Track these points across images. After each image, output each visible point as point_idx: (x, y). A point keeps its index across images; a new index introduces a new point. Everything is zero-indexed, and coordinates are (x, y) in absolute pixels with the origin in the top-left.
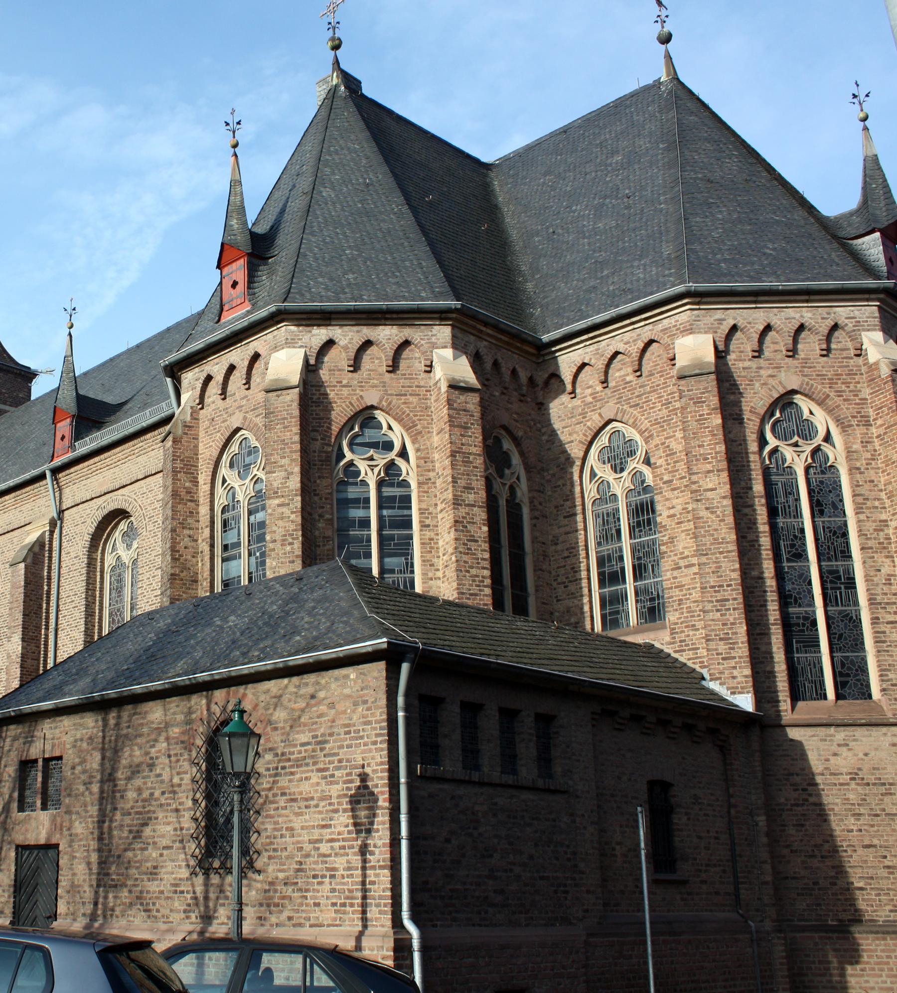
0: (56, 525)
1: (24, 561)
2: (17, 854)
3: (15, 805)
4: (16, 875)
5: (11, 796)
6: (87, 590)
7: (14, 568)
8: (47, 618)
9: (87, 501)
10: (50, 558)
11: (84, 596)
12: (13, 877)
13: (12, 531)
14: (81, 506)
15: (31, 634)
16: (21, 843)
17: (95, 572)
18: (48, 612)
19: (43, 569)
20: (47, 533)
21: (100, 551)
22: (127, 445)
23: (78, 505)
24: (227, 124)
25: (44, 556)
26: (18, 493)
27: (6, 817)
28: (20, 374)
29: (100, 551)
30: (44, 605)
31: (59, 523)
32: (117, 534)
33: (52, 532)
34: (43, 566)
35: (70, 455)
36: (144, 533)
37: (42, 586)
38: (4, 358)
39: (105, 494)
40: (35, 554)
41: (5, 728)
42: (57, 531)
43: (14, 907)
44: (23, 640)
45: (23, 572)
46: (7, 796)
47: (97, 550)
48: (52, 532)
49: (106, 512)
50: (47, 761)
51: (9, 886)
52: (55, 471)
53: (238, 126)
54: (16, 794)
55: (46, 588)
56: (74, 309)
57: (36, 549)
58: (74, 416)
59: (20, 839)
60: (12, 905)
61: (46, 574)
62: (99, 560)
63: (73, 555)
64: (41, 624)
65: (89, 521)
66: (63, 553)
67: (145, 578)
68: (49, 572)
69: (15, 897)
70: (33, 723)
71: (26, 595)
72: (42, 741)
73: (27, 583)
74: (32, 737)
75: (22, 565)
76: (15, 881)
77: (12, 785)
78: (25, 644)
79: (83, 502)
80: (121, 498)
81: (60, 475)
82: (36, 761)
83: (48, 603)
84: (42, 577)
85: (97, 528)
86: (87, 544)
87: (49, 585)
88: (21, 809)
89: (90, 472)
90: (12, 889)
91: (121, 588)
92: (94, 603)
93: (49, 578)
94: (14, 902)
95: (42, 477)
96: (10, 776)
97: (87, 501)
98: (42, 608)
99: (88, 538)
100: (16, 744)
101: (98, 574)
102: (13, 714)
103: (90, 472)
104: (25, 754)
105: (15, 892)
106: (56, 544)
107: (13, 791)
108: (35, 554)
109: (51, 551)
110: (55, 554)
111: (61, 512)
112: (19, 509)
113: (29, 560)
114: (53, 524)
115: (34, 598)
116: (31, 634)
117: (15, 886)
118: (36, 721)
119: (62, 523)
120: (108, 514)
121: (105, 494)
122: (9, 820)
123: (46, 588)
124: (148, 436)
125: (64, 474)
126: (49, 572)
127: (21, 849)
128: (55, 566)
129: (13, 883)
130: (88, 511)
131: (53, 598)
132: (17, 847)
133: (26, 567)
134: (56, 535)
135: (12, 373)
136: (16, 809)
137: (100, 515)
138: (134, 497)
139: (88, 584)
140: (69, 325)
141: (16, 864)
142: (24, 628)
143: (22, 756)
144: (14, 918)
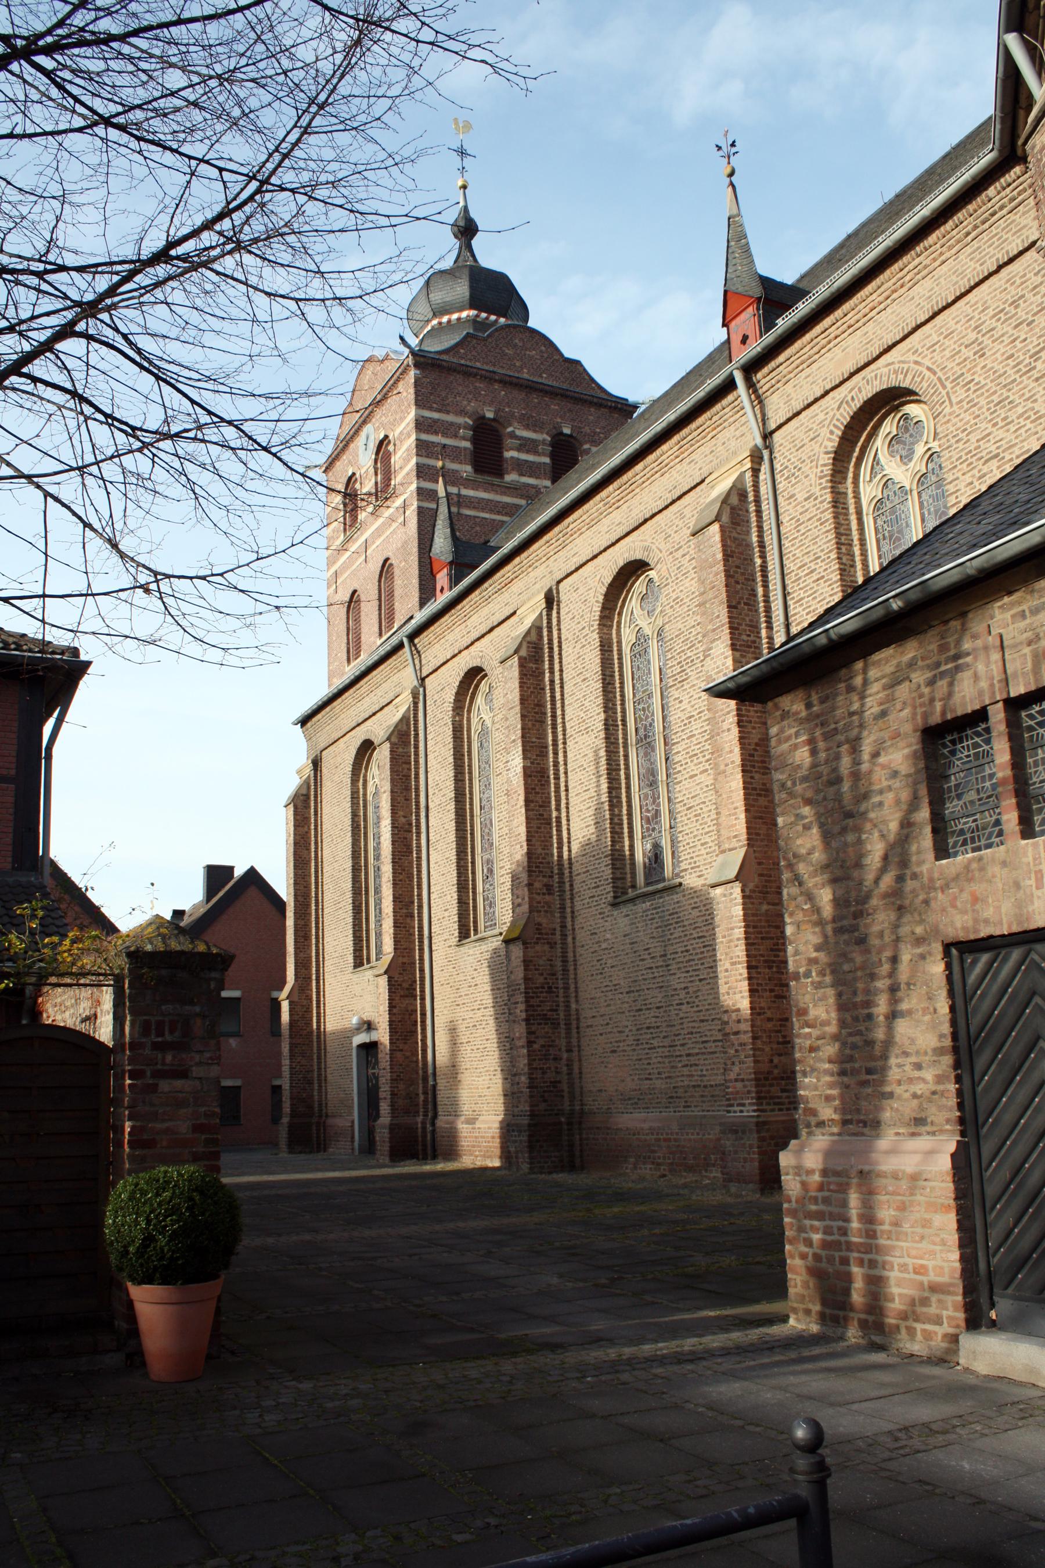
0: (761, 458)
1: (717, 519)
2: (948, 966)
3: (926, 840)
4: (954, 1023)
5: (907, 824)
6: (839, 544)
7: (700, 537)
8: (768, 610)
9: (816, 400)
10: (759, 512)
11: (833, 555)
12: (946, 1028)
13: (679, 498)
14: (804, 414)
15: (744, 637)
16: (962, 936)
17: (847, 514)
18: (767, 601)
19: (748, 533)
20: (748, 474)
21: (850, 480)
22: (887, 273)
23: (798, 413)
24: (719, 148)
25: (747, 511)
26: (684, 432)
27: (900, 879)
28: (616, 408)
29: (850, 480)
30: (760, 591)
31: (766, 454)
32: (880, 443)
33: (756, 472)
34: (749, 527)
35: (770, 337)
36: (947, 410)
37: (752, 560)
38: (593, 389)
39: (852, 375)
40: (733, 508)
41: (859, 665)
42: (765, 468)
43: (960, 1106)
44: (734, 647)
45: (718, 538)
46: (893, 826)
47: (845, 478)
48: (756, 472)
49: (857, 404)
50: (1015, 705)
51: (939, 1051)
52: (751, 368)
53: (734, 150)
54: (924, 814)
55: (758, 561)
56: (733, 145)
57: (734, 500)
58: (759, 299)
59: (959, 924)
60: (953, 1101)
61: (755, 539)
62: (850, 495)
63: (800, 497)
64: (758, 622)
65: (824, 432)
66: (780, 499)
67: (962, 486)
68: (761, 536)
69: (958, 1079)
70: (955, 624)
71: (728, 575)
72: (996, 656)
73: (727, 556)
74: (957, 657)
75: (715, 528)
76: (955, 1036)
77: (905, 795)
78: (738, 654)
79: (809, 406)
80: (886, 370)
81: (759, 375)
82: (981, 715)
83: (766, 586)
84: (749, 545)
85: (844, 438)
86: (828, 470)
87: (763, 556)
88: (942, 851)
89: (816, 349)
90: (948, 1060)
91: (900, 532)
92: (853, 566)
93: (762, 545)
94: (960, 1093)
95: (729, 385)
96: (895, 774)
97: (816, 400)
98: (755, 596)
99: (827, 459)
100: (903, 691)
101: (625, 818)
102: (896, 605)
103: (816, 349)
104: (938, 706)
105: (957, 1065)
106: (765, 489)
107: (913, 806)
108: (733, 508)
109: (757, 501)
110: (767, 507)
111: (767, 436)
112: (687, 460)
113: (725, 518)
114: (756, 457)
115: (741, 579)
116: (744, 637)
117: (955, 1050)
118: (963, 615)
119: (771, 453)
120: (861, 409)
121: (852, 375)
122: (910, 885)
123: (758, 561)
124: (932, 238)
125: (765, 370)
126: (761, 536)
127: (961, 950)
128: (769, 523)
129: (948, 1042)
130: (821, 416)
131: (774, 577)
132: (947, 947)
133: (723, 529)
134: (764, 475)
135: (606, 407)
136: (930, 855)
137: (844, 416)
138: (915, 358)
139: (838, 535)
140: (729, 170)
141: (951, 994)
142: (733, 629)
143: (925, 716)
144: (963, 1134)
